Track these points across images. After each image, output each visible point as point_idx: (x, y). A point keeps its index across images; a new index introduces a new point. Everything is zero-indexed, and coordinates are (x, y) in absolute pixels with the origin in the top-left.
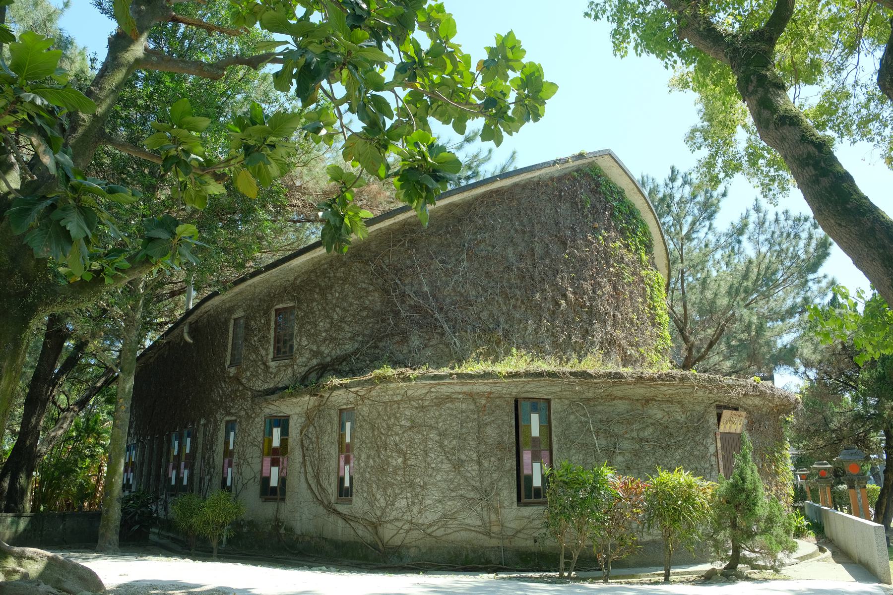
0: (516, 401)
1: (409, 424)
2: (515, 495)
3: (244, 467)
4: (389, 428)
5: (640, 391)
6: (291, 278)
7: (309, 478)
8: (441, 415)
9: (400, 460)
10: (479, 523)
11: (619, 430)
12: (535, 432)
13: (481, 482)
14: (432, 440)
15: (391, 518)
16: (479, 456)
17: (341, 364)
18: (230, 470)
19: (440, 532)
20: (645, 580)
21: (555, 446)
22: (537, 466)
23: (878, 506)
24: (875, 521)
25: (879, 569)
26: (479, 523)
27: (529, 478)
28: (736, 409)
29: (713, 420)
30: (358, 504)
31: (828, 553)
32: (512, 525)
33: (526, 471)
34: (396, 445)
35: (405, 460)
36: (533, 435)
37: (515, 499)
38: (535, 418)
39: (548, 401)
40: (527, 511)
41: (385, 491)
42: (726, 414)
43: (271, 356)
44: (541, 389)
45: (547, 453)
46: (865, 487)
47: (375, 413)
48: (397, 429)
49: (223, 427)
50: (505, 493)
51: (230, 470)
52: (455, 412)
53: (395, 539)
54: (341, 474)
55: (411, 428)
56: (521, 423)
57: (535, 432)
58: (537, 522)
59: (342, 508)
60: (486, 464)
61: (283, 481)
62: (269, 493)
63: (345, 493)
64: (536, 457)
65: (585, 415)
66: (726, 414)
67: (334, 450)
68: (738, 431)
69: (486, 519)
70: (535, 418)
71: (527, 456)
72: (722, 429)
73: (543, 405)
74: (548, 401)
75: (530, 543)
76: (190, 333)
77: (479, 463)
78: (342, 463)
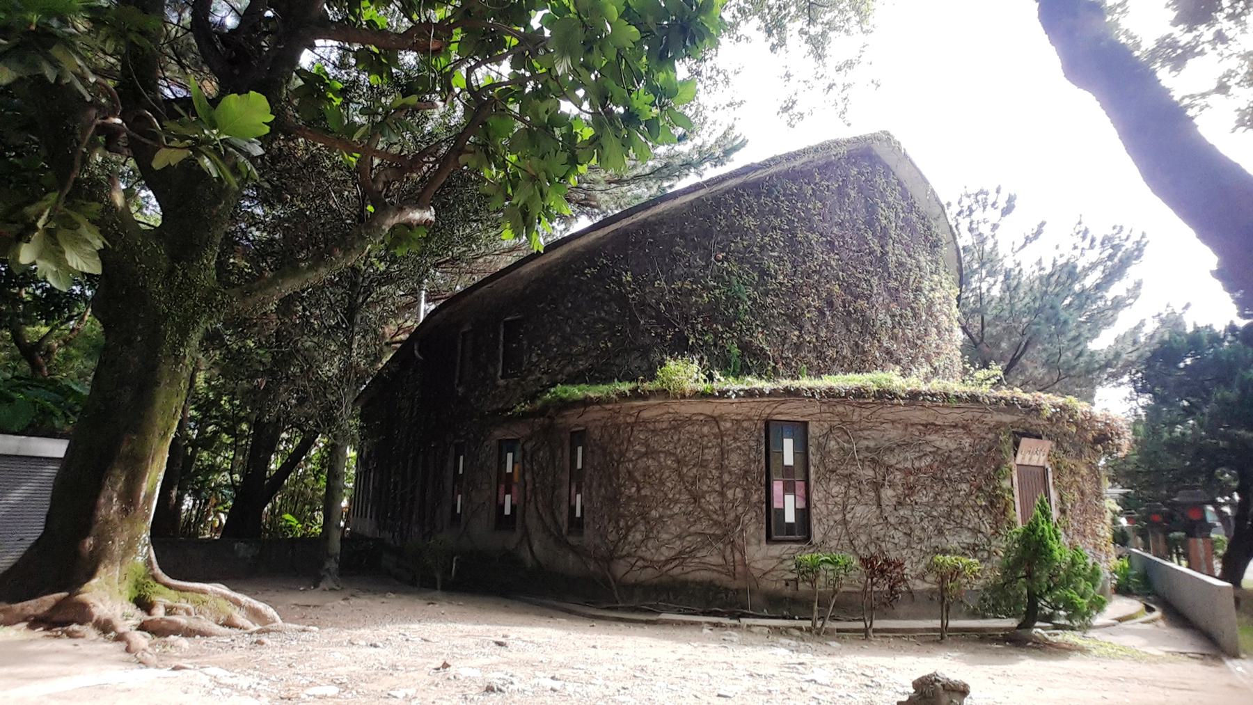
0: (767, 423)
1: (643, 450)
2: (764, 531)
3: (473, 494)
4: (622, 454)
5: (918, 415)
6: (520, 287)
7: (540, 506)
8: (679, 440)
9: (634, 489)
10: (721, 561)
11: (891, 460)
12: (789, 459)
13: (725, 515)
14: (669, 468)
15: (624, 553)
16: (723, 486)
17: (980, 385)
18: (508, 497)
19: (678, 571)
20: (243, 598)
21: (812, 476)
22: (790, 499)
23: (1225, 560)
24: (1219, 578)
25: (1224, 640)
26: (721, 561)
27: (782, 512)
28: (1039, 437)
29: (1008, 447)
30: (589, 537)
31: (1157, 614)
32: (759, 565)
33: (777, 504)
34: (629, 472)
35: (639, 490)
36: (786, 463)
37: (764, 536)
38: (788, 444)
39: (806, 424)
40: (776, 550)
41: (617, 522)
42: (1025, 442)
43: (500, 373)
44: (791, 411)
45: (802, 484)
46: (1208, 537)
47: (606, 437)
48: (630, 455)
49: (452, 450)
50: (752, 529)
51: (579, 497)
52: (696, 437)
53: (628, 576)
54: (501, 502)
55: (646, 454)
56: (772, 449)
57: (789, 459)
58: (790, 563)
59: (573, 540)
60: (730, 494)
61: (804, 514)
62: (504, 523)
63: (577, 525)
64: (789, 488)
65: (849, 442)
66: (1025, 442)
67: (566, 477)
68: (1041, 464)
69: (730, 558)
70: (788, 444)
71: (778, 487)
72: (1019, 460)
73: (800, 430)
74: (806, 424)
75: (780, 586)
76: (419, 350)
77: (722, 494)
78: (573, 490)
